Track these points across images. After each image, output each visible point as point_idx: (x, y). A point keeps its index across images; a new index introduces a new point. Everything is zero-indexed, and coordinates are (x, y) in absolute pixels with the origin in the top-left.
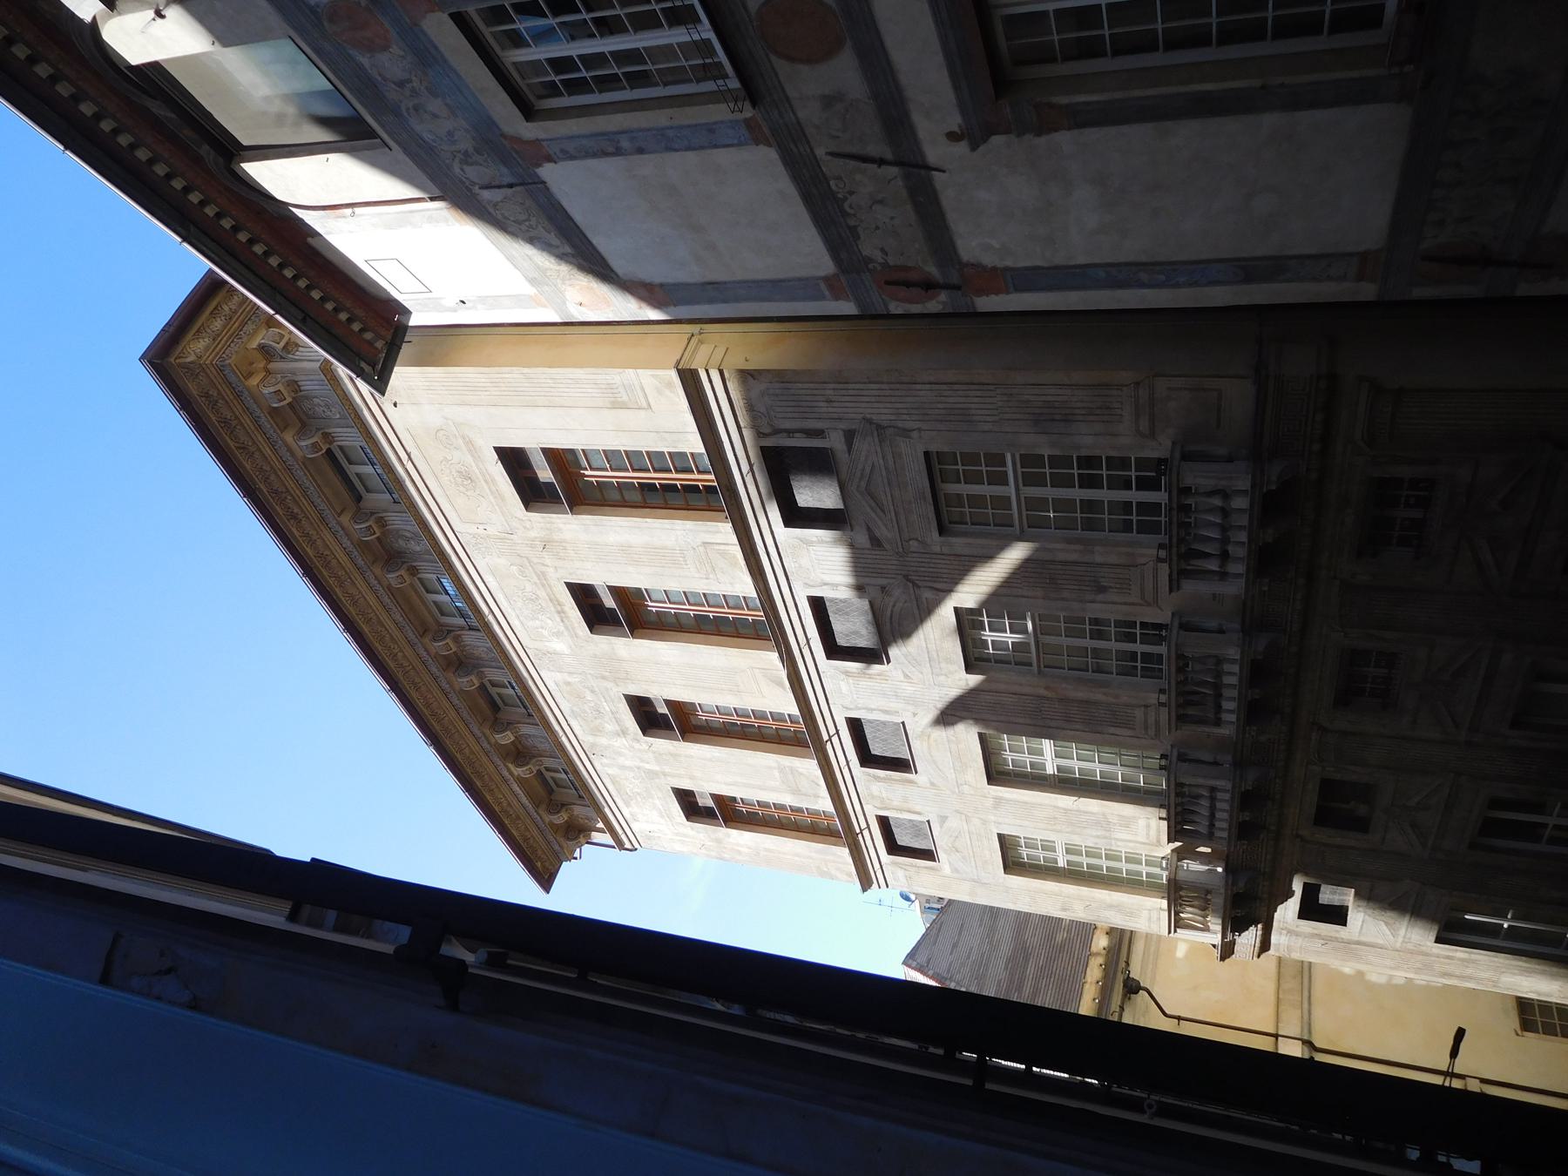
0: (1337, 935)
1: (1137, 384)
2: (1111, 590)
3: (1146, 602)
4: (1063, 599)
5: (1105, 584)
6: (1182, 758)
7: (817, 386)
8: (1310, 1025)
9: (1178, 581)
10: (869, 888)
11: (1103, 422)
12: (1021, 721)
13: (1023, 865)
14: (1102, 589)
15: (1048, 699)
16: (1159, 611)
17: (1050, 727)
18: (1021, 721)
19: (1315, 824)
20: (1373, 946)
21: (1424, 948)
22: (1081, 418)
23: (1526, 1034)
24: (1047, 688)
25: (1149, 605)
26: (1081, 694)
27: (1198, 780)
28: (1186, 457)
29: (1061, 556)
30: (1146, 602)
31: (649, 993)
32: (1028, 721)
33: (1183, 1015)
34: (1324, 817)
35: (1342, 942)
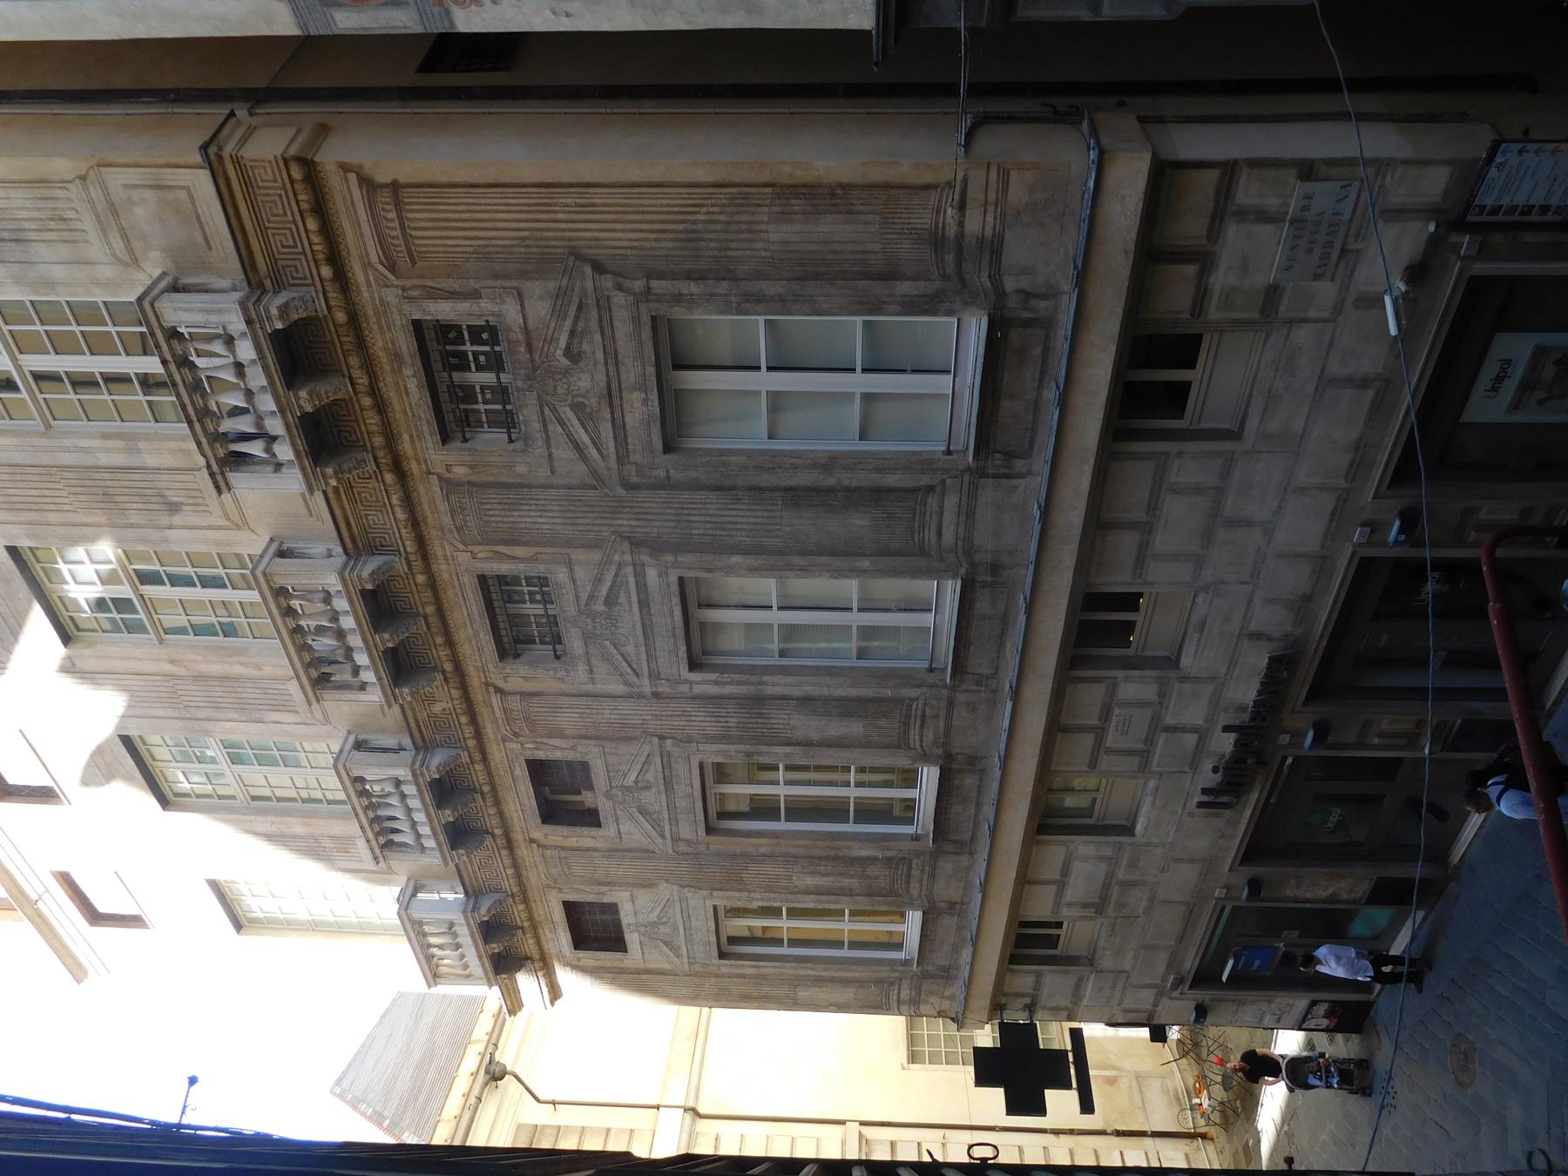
0: (623, 965)
1: (83, 178)
2: (186, 508)
3: (232, 522)
4: (131, 526)
5: (175, 499)
6: (359, 746)
7: (590, 509)
8: (698, 1089)
9: (223, 474)
10: (520, 1010)
11: (67, 241)
12: (161, 713)
13: (257, 921)
14: (174, 508)
15: (179, 677)
16: (255, 537)
17: (198, 719)
18: (161, 713)
19: (543, 822)
20: (658, 974)
21: (712, 968)
22: (33, 236)
23: (912, 1066)
24: (172, 661)
25: (239, 528)
26: (215, 668)
27: (377, 773)
28: (175, 288)
29: (104, 460)
30: (232, 522)
31: (245, 1166)
32: (171, 713)
33: (558, 1099)
34: (552, 813)
35: (631, 973)
